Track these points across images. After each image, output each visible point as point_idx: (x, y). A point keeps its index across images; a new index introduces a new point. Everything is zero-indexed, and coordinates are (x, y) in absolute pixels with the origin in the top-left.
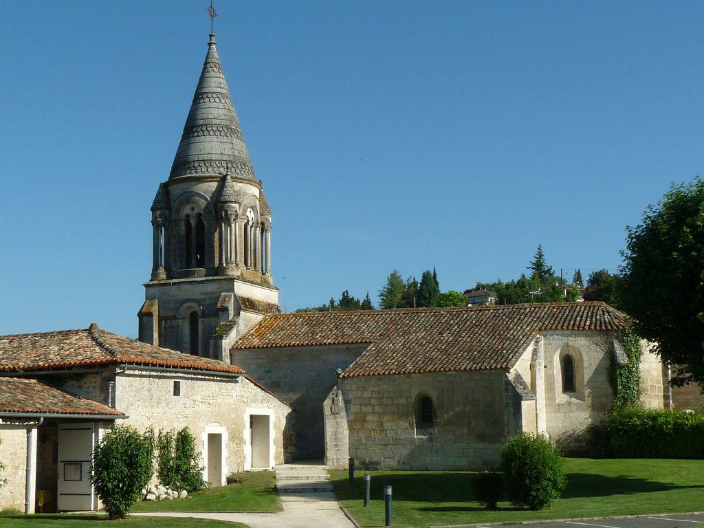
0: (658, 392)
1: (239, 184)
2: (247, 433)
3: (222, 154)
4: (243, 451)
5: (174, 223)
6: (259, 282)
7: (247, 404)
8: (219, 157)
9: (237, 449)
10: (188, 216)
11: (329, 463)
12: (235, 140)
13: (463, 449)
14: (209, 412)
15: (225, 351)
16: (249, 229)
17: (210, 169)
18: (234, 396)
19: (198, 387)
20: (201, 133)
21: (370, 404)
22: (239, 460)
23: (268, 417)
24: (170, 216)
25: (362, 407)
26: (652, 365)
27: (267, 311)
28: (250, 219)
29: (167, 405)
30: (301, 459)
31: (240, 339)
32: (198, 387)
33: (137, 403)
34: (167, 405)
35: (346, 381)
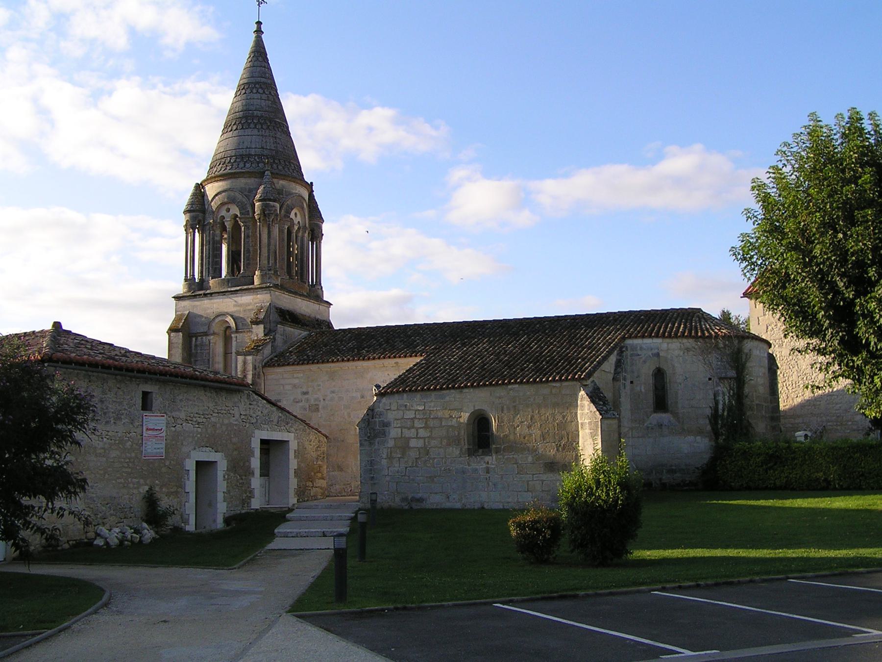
0: (766, 412)
1: (281, 182)
2: (255, 463)
3: (262, 148)
5: (208, 227)
6: (305, 294)
7: (257, 426)
8: (259, 151)
9: (241, 481)
10: (223, 217)
12: (279, 133)
13: (528, 481)
18: (237, 416)
19: (181, 400)
21: (413, 427)
24: (204, 219)
25: (403, 430)
26: (759, 379)
27: (314, 327)
28: (296, 222)
31: (276, 357)
32: (181, 400)
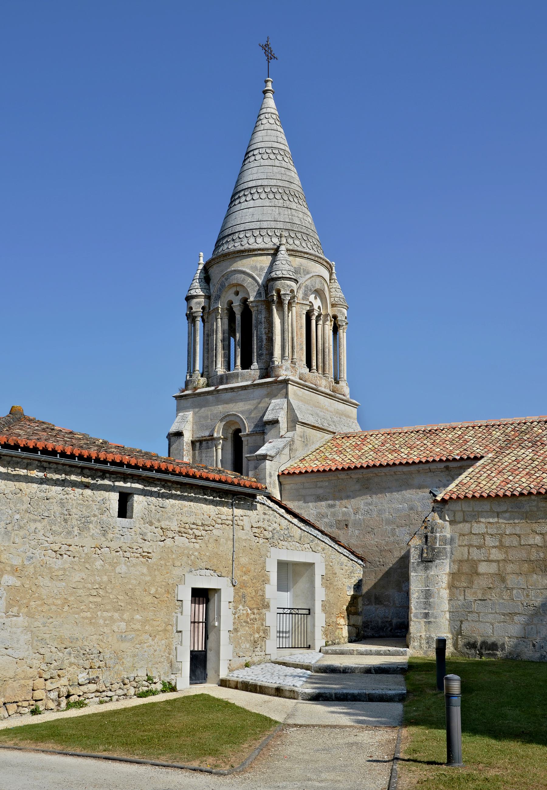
4: (264, 620)
11: (414, 644)
14: (197, 550)
15: (271, 476)
16: (314, 322)
17: (259, 240)
20: (249, 198)
22: (257, 635)
23: (311, 565)
28: (316, 307)
29: (105, 533)
30: (380, 637)
33: (33, 526)
34: (105, 533)
35: (447, 507)
